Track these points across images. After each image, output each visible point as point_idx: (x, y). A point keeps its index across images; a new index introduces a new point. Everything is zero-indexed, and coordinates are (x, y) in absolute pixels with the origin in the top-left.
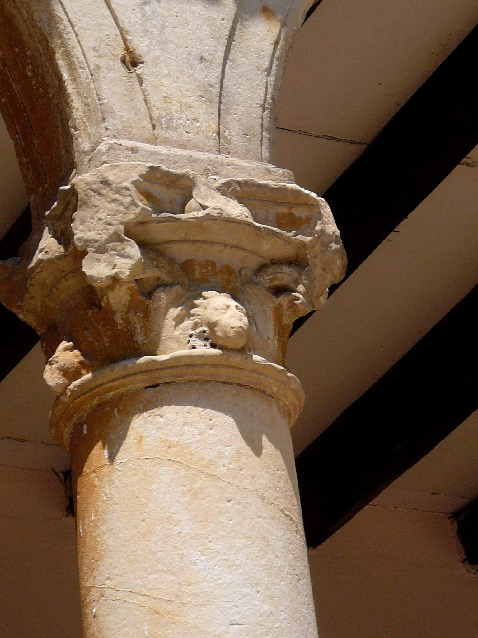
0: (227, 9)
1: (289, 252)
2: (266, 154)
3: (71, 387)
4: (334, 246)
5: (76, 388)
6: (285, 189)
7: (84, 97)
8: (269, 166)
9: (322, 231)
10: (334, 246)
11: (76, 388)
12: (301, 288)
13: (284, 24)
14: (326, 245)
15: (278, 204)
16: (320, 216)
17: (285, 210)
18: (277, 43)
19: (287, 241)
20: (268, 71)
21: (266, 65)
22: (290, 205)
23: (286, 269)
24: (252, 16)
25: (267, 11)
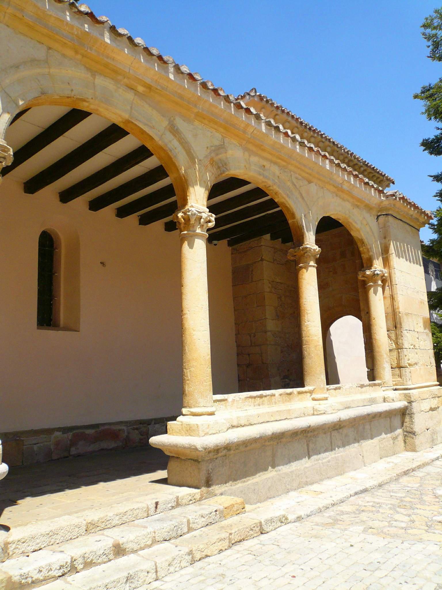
0: (100, 524)
1: (3, 156)
2: (3, 138)
3: (299, 140)
4: (12, 156)
5: (435, 350)
6: (4, 145)
7: (439, 352)
8: (3, 140)
9: (9, 154)
10: (12, 156)
11: (435, 350)
12: (4, 162)
13: (11, 115)
14: (10, 156)
15: (2, 147)
16: (10, 151)
17: (4, 149)
18: (9, 119)
19: (3, 154)
20: (6, 123)
21: (6, 122)
22: (4, 148)
23: (2, 159)
24: (5, 113)
25: (8, 113)
